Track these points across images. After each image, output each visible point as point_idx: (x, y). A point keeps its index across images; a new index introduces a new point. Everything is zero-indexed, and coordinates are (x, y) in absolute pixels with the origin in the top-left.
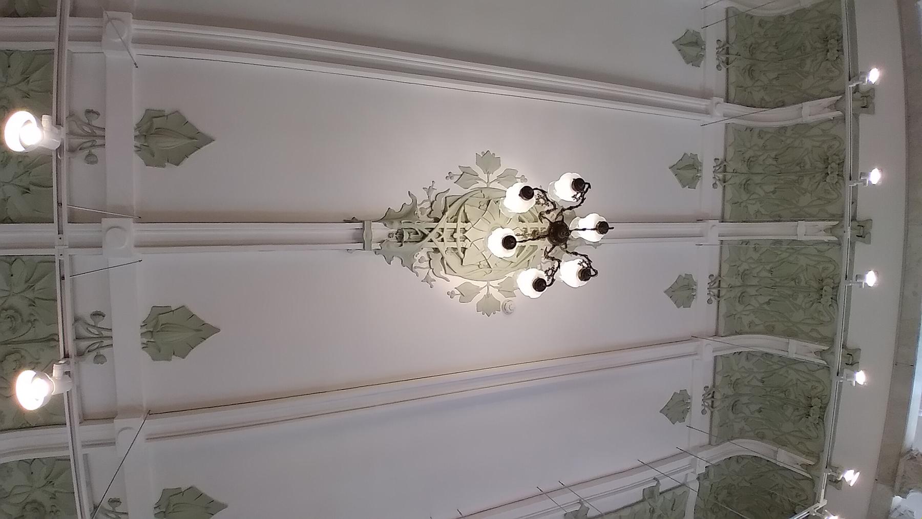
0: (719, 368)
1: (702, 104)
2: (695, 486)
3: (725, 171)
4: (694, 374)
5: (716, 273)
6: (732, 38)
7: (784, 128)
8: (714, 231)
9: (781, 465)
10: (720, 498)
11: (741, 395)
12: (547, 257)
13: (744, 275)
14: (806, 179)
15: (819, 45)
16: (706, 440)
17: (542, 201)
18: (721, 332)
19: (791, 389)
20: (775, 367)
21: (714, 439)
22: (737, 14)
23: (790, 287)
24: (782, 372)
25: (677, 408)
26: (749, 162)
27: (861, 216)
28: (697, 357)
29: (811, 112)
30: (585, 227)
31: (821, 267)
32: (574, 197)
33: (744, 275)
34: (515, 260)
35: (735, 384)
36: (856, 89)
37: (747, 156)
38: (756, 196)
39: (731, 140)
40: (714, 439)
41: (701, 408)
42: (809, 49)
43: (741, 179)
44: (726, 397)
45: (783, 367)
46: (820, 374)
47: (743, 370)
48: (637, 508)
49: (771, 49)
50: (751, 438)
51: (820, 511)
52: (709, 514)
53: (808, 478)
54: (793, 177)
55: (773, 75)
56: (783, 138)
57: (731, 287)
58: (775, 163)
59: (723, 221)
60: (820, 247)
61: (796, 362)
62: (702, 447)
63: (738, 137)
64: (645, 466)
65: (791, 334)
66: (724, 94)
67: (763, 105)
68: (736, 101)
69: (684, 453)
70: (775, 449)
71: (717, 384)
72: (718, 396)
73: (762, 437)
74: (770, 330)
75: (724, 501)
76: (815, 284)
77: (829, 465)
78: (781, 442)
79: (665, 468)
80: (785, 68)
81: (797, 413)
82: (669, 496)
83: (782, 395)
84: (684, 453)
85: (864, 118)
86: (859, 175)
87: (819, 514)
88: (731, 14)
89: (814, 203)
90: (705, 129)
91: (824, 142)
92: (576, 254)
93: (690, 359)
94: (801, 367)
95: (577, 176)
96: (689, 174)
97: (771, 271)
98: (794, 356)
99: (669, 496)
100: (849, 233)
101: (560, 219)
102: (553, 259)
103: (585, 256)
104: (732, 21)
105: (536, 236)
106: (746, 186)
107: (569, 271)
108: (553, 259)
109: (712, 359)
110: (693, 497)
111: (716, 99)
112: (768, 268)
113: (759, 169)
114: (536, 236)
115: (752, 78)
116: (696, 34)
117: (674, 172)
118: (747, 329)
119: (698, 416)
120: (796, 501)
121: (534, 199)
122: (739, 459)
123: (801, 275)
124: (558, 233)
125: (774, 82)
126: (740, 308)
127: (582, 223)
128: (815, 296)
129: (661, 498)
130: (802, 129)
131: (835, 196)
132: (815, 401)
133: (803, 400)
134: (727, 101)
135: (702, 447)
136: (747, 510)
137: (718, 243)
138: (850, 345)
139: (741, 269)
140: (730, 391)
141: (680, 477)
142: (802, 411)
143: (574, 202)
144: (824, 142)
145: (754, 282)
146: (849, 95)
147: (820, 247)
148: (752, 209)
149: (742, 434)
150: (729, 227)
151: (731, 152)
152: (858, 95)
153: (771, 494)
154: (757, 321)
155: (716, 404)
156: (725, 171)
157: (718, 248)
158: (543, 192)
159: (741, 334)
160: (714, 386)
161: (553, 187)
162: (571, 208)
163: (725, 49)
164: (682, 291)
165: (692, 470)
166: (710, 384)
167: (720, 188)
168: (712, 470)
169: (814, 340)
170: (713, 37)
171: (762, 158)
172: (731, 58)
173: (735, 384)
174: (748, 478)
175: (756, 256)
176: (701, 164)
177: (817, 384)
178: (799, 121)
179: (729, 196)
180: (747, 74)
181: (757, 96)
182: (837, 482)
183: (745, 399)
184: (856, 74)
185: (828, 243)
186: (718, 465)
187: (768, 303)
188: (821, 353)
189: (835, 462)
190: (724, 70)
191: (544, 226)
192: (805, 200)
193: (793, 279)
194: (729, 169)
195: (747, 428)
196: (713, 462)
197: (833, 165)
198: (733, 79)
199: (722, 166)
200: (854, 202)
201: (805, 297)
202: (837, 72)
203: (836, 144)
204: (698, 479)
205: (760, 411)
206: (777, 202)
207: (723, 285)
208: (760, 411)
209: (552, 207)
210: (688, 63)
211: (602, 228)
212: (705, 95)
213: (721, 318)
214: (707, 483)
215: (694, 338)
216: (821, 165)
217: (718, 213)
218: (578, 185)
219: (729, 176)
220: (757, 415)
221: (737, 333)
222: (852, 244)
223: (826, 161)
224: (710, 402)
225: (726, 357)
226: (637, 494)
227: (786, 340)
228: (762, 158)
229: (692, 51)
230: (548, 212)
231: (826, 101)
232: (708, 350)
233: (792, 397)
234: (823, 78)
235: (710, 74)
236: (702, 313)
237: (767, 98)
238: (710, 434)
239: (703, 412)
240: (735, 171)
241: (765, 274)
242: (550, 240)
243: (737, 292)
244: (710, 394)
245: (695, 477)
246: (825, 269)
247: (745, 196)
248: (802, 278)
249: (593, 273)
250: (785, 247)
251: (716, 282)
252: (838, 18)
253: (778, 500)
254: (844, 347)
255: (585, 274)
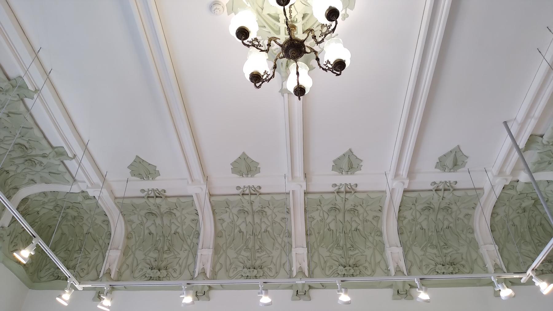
0: (182, 200)
1: (404, 172)
2: (75, 189)
3: (347, 192)
4: (175, 180)
5: (262, 191)
6: (457, 193)
7: (381, 235)
8: (297, 187)
9: (107, 254)
10: (69, 211)
11: (162, 218)
12: (270, 40)
13: (262, 212)
14: (340, 252)
15: (448, 259)
16: (119, 194)
17: (325, 29)
18: (213, 199)
19: (172, 254)
20: (189, 241)
21: (121, 201)
22: (478, 197)
23: (254, 246)
24: (186, 247)
25: (142, 169)
26: (354, 210)
27: (313, 292)
28: (190, 182)
29: (394, 253)
30: (301, 73)
31: (272, 266)
32: (328, 62)
33: (262, 212)
34: (265, 12)
35: (170, 213)
36: (412, 286)
37: (359, 208)
38: (326, 217)
39: (372, 196)
40: (121, 201)
41: (146, 189)
42: (445, 251)
43: (340, 205)
44: (158, 207)
45: (189, 246)
46: (187, 274)
47: (183, 218)
48: (44, 142)
49: (446, 223)
50: (126, 229)
51: (73, 287)
52: (53, 204)
53: (98, 275)
54: (341, 243)
55: (425, 225)
56: (373, 235)
57: (251, 203)
58: (353, 229)
59: (306, 193)
60: (287, 265)
61: (195, 256)
62: (112, 192)
63: (375, 202)
64: (85, 147)
65: (217, 250)
66: (412, 188)
67: (400, 219)
68: (404, 198)
69: (103, 178)
70: (120, 248)
71: (169, 199)
72: (158, 200)
73: (128, 237)
74: (218, 235)
75: (67, 214)
76: (258, 263)
77: (113, 288)
78: (126, 251)
79: (86, 163)
80: (430, 234)
81: (152, 260)
82: (61, 168)
83: (166, 248)
84: (103, 178)
85: (389, 292)
86: (346, 288)
87: (69, 285)
88: (478, 192)
89: (321, 258)
90: (383, 176)
91: (370, 263)
92: (275, 67)
93: (187, 175)
94: (190, 260)
95: (348, 63)
96: (345, 166)
97: (266, 231)
98: (199, 254)
99: (61, 168)
100: (300, 282)
101: (308, 50)
102: (269, 45)
103: (273, 76)
104: (472, 193)
105: (291, 28)
106: (335, 208)
107: (259, 62)
108: (269, 45)
109: (189, 193)
110: (64, 188)
111: (407, 182)
112: (269, 229)
113: (348, 218)
114: (291, 28)
115: (423, 210)
116: (464, 164)
117: (347, 153)
118: (218, 218)
119: (137, 187)
120: (77, 269)
121: (328, 23)
122: (107, 222)
123: (264, 253)
124: (294, 49)
125: (419, 226)
126: (235, 211)
127: (304, 70)
128: (248, 264)
129: (58, 162)
130: (380, 247)
131: (328, 273)
132: (164, 272)
133: (164, 264)
134: (405, 191)
135: (112, 192)
136: (63, 234)
137: (287, 191)
138: (212, 293)
139: (266, 210)
140: (164, 209)
141: (80, 176)
142: (154, 264)
143: (323, 62)
144: (370, 263)
145: (257, 220)
146: (407, 278)
147: (287, 265)
148: (316, 215)
149: (128, 222)
150: (300, 198)
151: (363, 196)
152: (408, 287)
153: (80, 249)
154: (225, 225)
155: (151, 200)
156: (347, 192)
157: (284, 191)
158: (334, 30)
159: (213, 214)
160: (166, 197)
161: (338, 41)
162: (318, 59)
163: (449, 188)
164: (245, 166)
165: (89, 185)
166: (167, 194)
167: (332, 189)
168: (93, 201)
169: (213, 268)
170: (461, 179)
171: (357, 220)
172: (441, 193)
173: (170, 213)
174: (91, 230)
175: (278, 219)
176: (352, 174)
177: (178, 272)
178: (387, 245)
179: (326, 196)
180: (427, 205)
181: (408, 214)
182: (99, 297)
183: (158, 221)
184: (425, 283)
185: (291, 270)
186: (98, 207)
187: (240, 231)
188: (203, 272)
189: (115, 293)
190: (431, 188)
191: (300, 35)
192: (324, 252)
193: (261, 248)
194: (348, 195)
195: (134, 226)
196: (100, 202)
197: (352, 271)
198: (423, 195)
199: (350, 190)
200: (323, 286)
201: (247, 257)
202: (426, 272)
203: (369, 273)
204: (83, 192)
205: (150, 233)
206: (322, 232)
207: (253, 197)
208: (150, 233)
209: (320, 39)
210: (439, 159)
211: (300, 91)
212: (411, 174)
213: (225, 197)
214: (80, 199)
215: (207, 178)
216: (352, 262)
217: (312, 189)
218: (340, 65)
219: (343, 195)
220: (147, 232)
221: (214, 211)
222: (291, 287)
223: (355, 265)
224: (152, 195)
225: (193, 204)
226: (57, 141)
227: (211, 246)
228: (357, 220)
229: (449, 162)
230: (314, 37)
231: (402, 264)
232: (197, 190)
233: (165, 256)
234: (421, 261)
235: (429, 176)
236: (228, 183)
237: (405, 222)
238: (124, 198)
239: (143, 191)
240: (346, 199)
241: (264, 227)
242: (286, 42)
243: (248, 207)
244: (159, 195)
245: (84, 189)
246: (270, 269)
247: (326, 208)
248: (262, 254)
249: (258, 85)
250: (286, 240)
251: (255, 192)
252: (472, 271)
253: (76, 255)
254: (210, 288)
255: (256, 78)
